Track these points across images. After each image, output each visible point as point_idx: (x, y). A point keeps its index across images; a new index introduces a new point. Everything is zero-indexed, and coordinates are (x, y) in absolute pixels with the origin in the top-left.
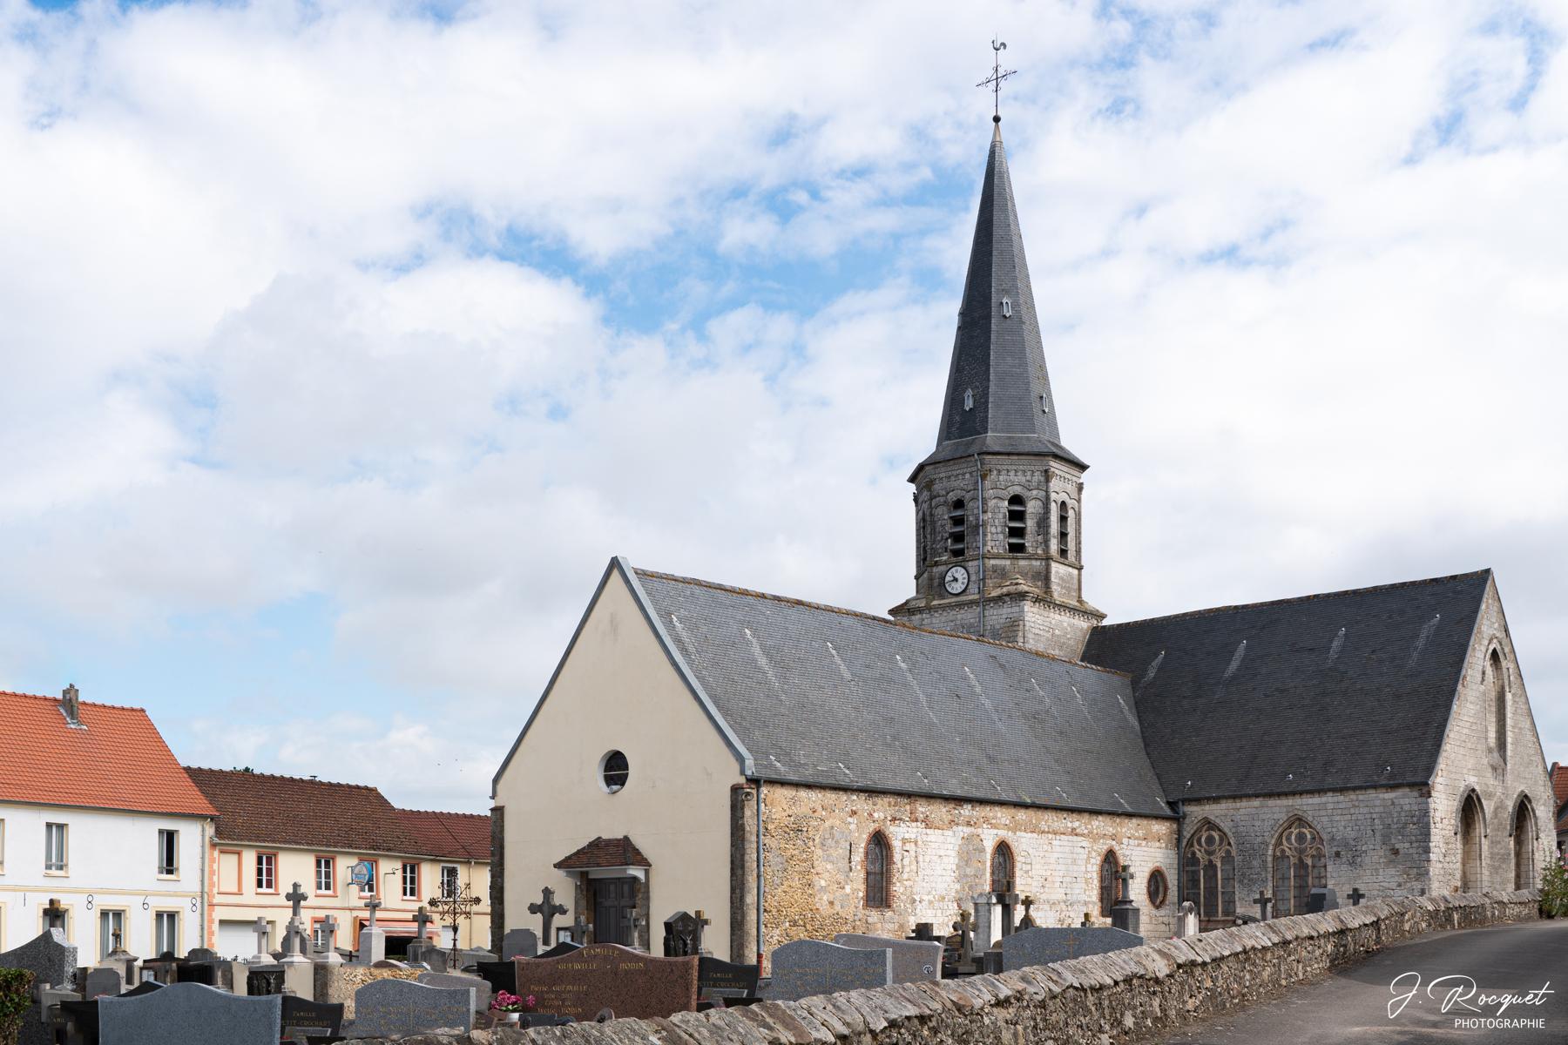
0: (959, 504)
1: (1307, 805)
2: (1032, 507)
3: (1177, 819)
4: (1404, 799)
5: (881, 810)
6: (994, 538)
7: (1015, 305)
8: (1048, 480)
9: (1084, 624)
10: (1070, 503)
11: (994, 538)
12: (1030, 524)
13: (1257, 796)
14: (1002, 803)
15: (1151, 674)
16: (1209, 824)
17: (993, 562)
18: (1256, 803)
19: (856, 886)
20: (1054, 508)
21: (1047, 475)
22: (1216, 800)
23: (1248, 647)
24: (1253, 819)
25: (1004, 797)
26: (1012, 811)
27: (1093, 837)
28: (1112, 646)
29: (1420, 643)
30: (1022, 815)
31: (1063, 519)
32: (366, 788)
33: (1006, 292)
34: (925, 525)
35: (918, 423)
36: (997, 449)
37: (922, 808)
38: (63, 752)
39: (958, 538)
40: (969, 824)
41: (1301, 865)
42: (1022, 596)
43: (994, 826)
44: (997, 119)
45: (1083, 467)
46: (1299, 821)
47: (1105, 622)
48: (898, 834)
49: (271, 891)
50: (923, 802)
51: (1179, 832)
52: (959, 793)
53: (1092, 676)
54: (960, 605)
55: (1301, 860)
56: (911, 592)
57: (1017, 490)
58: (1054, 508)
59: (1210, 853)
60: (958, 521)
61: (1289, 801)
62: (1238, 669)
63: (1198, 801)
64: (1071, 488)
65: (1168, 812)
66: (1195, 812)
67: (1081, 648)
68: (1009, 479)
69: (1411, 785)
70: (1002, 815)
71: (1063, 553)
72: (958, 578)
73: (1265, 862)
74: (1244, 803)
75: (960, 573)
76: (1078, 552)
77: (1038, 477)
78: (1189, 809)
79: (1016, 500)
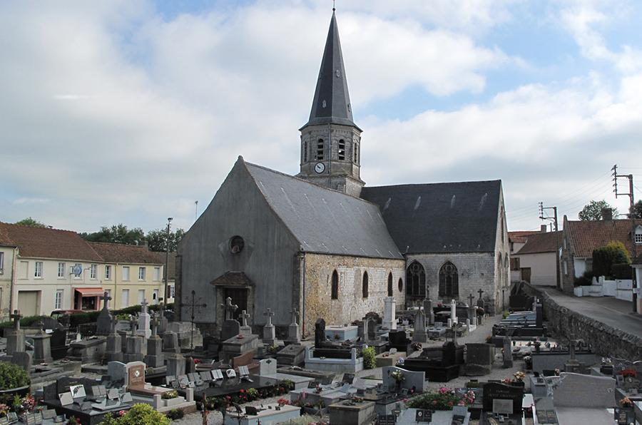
0: (321, 141)
1: (452, 257)
2: (347, 144)
3: (405, 260)
4: (486, 256)
5: (336, 260)
6: (335, 152)
7: (341, 73)
8: (352, 136)
9: (360, 186)
10: (358, 144)
11: (335, 152)
12: (346, 150)
13: (434, 253)
14: (365, 257)
15: (387, 206)
16: (416, 262)
17: (334, 163)
18: (434, 255)
19: (329, 293)
20: (354, 145)
21: (352, 134)
22: (419, 254)
23: (421, 199)
24: (432, 262)
25: (367, 255)
26: (368, 259)
27: (387, 268)
28: (369, 194)
29: (482, 203)
30: (370, 261)
31: (356, 149)
32: (73, 232)
33: (338, 68)
34: (305, 146)
35: (303, 110)
36: (336, 122)
37: (347, 260)
38: (33, 240)
39: (320, 152)
40: (357, 266)
41: (449, 278)
42: (346, 176)
43: (363, 266)
44: (334, 9)
45: (361, 131)
46: (449, 263)
47: (365, 186)
48: (340, 270)
49: (40, 277)
50: (346, 257)
51: (406, 265)
52: (355, 254)
53: (363, 202)
54: (321, 177)
55: (449, 276)
56: (568, 220)
57: (342, 138)
58: (354, 145)
59: (416, 272)
60: (321, 147)
61: (446, 255)
62: (419, 207)
63: (413, 254)
64: (357, 138)
65: (403, 258)
66: (412, 258)
67: (359, 195)
68: (339, 134)
69: (488, 252)
70: (365, 261)
71: (356, 161)
72: (320, 168)
73: (436, 276)
74: (430, 255)
75: (321, 165)
76: (359, 161)
77: (349, 135)
78: (409, 256)
79: (342, 141)
